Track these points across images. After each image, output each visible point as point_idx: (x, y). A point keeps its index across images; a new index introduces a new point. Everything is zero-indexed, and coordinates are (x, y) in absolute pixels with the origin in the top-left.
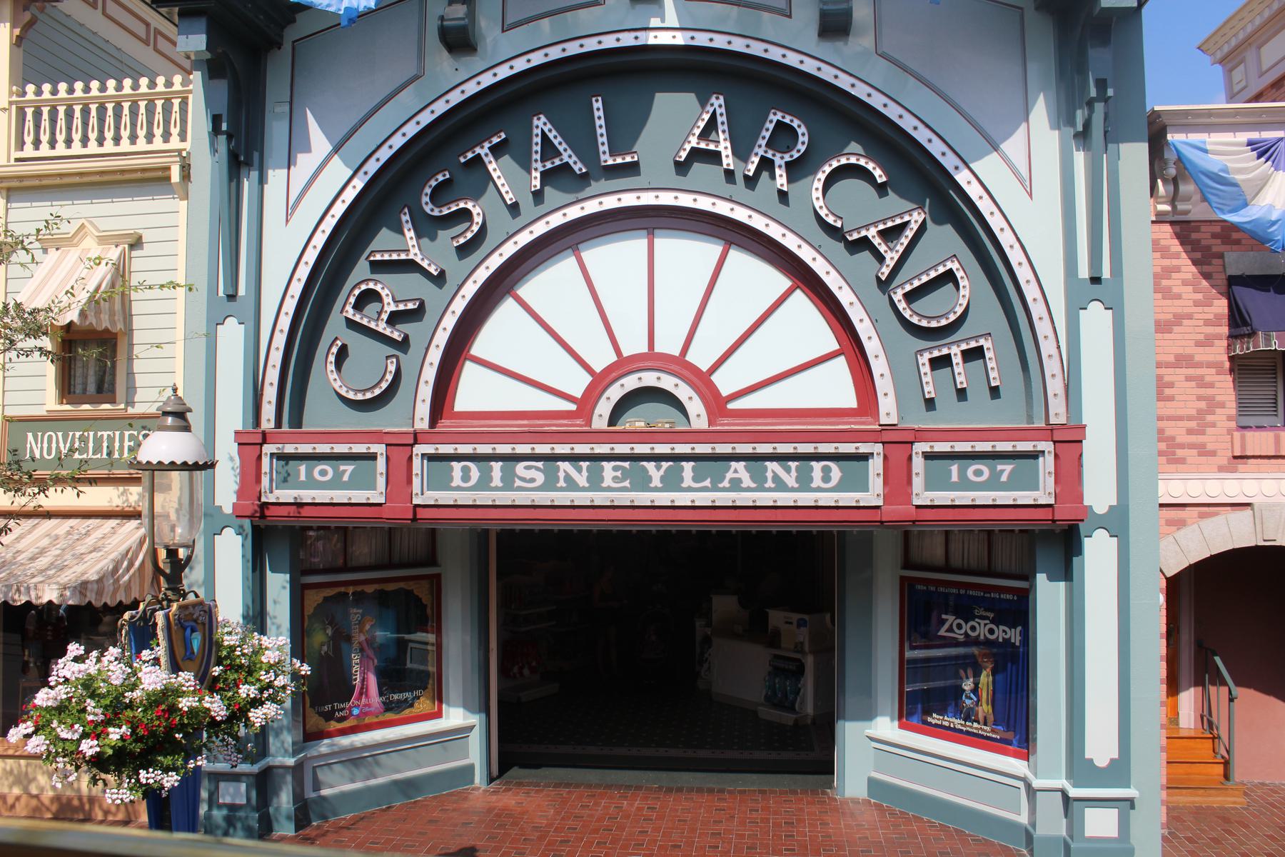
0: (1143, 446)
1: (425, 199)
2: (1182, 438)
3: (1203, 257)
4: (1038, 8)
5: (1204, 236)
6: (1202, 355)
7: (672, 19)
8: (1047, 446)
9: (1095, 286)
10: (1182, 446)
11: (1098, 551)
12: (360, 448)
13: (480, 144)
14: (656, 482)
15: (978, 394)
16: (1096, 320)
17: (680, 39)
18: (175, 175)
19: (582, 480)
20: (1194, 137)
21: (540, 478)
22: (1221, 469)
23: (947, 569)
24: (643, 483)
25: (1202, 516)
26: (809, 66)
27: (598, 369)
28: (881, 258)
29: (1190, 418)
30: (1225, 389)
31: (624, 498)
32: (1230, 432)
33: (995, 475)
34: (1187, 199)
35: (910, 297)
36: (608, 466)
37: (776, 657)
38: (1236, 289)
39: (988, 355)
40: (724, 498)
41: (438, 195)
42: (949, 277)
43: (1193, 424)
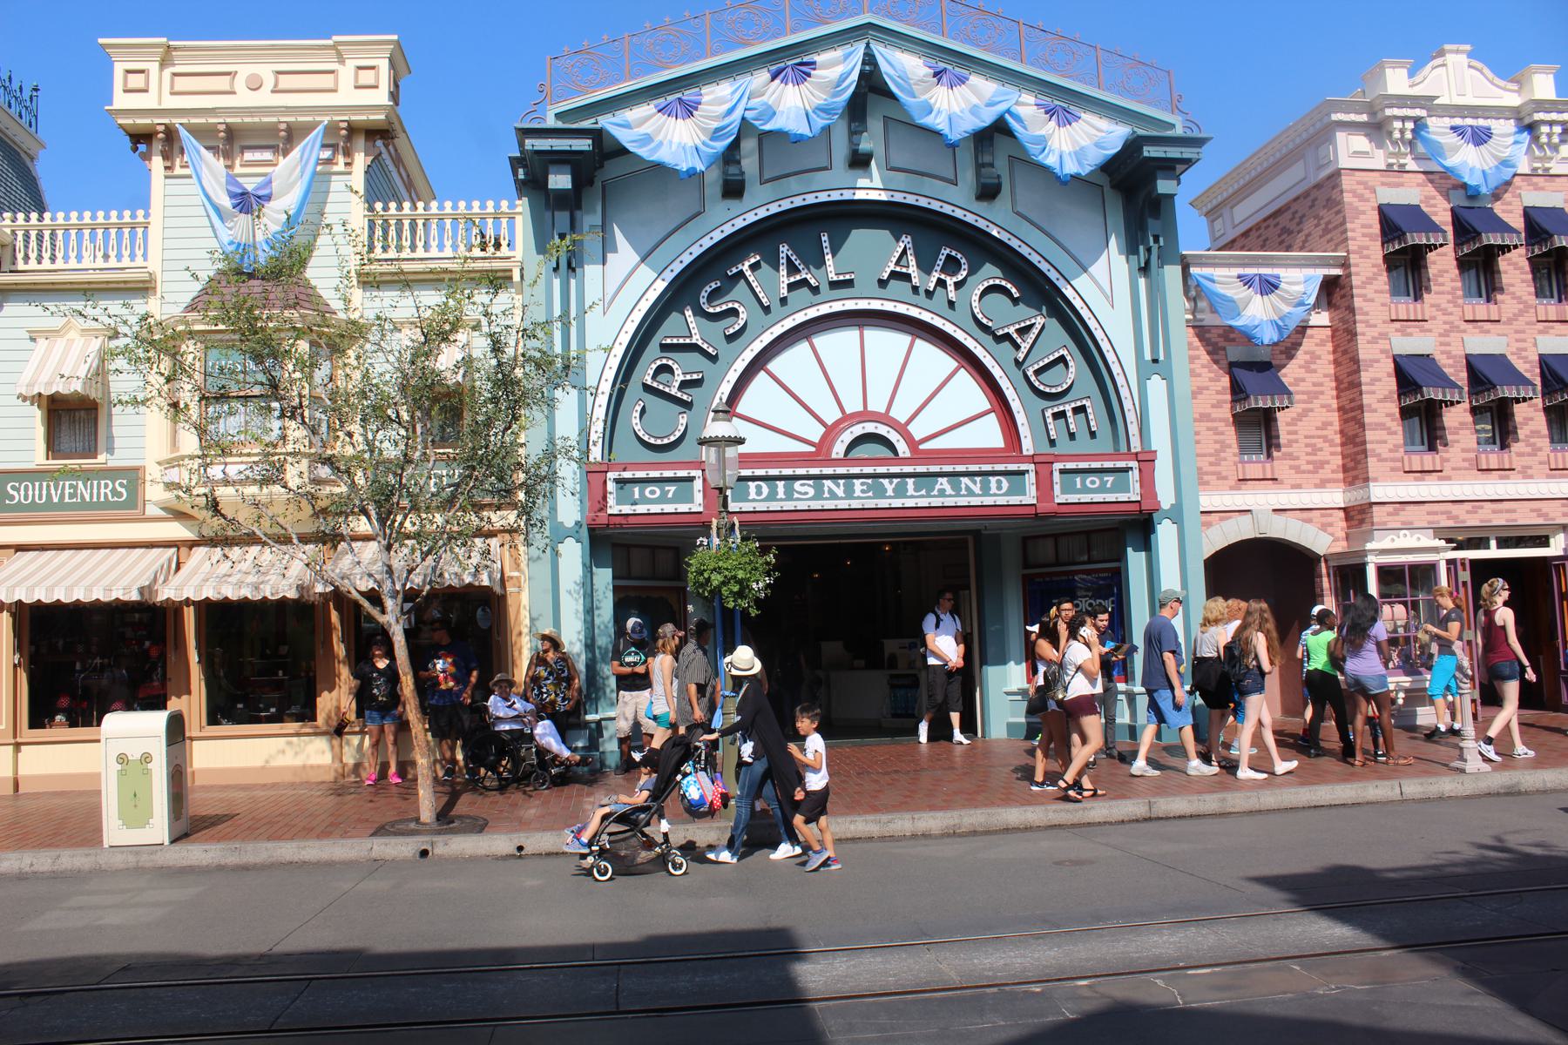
0: (1188, 472)
1: (704, 294)
2: (1207, 468)
3: (1214, 350)
4: (1113, 187)
5: (1213, 336)
6: (1216, 413)
7: (877, 183)
8: (1134, 464)
9: (1155, 364)
10: (1207, 473)
11: (1165, 533)
12: (682, 473)
13: (742, 262)
14: (890, 493)
15: (1083, 435)
16: (1156, 386)
17: (884, 196)
18: (516, 277)
19: (840, 492)
20: (1207, 271)
21: (811, 492)
22: (1231, 488)
23: (1058, 564)
24: (881, 493)
25: (1221, 519)
26: (970, 219)
27: (870, 408)
28: (1017, 347)
29: (1211, 455)
30: (1230, 434)
31: (870, 504)
32: (1235, 464)
33: (1103, 483)
34: (1202, 311)
35: (1037, 372)
36: (857, 482)
37: (892, 676)
38: (1235, 370)
39: (1089, 410)
40: (936, 502)
41: (714, 296)
42: (1062, 359)
43: (1212, 459)
